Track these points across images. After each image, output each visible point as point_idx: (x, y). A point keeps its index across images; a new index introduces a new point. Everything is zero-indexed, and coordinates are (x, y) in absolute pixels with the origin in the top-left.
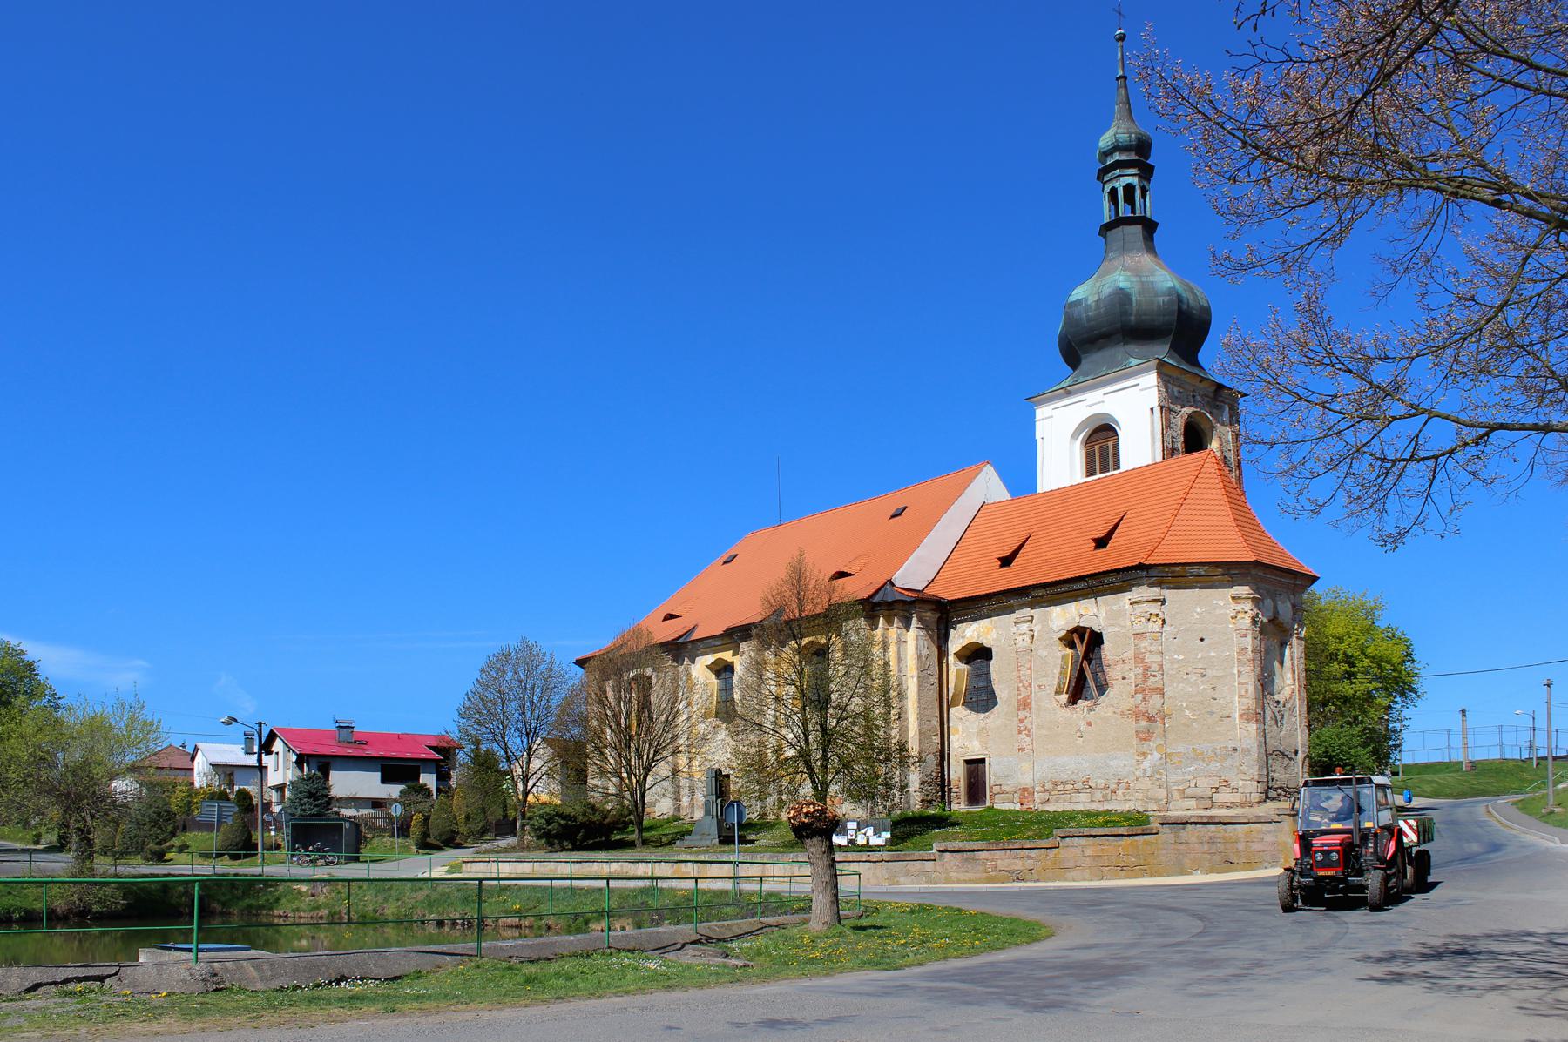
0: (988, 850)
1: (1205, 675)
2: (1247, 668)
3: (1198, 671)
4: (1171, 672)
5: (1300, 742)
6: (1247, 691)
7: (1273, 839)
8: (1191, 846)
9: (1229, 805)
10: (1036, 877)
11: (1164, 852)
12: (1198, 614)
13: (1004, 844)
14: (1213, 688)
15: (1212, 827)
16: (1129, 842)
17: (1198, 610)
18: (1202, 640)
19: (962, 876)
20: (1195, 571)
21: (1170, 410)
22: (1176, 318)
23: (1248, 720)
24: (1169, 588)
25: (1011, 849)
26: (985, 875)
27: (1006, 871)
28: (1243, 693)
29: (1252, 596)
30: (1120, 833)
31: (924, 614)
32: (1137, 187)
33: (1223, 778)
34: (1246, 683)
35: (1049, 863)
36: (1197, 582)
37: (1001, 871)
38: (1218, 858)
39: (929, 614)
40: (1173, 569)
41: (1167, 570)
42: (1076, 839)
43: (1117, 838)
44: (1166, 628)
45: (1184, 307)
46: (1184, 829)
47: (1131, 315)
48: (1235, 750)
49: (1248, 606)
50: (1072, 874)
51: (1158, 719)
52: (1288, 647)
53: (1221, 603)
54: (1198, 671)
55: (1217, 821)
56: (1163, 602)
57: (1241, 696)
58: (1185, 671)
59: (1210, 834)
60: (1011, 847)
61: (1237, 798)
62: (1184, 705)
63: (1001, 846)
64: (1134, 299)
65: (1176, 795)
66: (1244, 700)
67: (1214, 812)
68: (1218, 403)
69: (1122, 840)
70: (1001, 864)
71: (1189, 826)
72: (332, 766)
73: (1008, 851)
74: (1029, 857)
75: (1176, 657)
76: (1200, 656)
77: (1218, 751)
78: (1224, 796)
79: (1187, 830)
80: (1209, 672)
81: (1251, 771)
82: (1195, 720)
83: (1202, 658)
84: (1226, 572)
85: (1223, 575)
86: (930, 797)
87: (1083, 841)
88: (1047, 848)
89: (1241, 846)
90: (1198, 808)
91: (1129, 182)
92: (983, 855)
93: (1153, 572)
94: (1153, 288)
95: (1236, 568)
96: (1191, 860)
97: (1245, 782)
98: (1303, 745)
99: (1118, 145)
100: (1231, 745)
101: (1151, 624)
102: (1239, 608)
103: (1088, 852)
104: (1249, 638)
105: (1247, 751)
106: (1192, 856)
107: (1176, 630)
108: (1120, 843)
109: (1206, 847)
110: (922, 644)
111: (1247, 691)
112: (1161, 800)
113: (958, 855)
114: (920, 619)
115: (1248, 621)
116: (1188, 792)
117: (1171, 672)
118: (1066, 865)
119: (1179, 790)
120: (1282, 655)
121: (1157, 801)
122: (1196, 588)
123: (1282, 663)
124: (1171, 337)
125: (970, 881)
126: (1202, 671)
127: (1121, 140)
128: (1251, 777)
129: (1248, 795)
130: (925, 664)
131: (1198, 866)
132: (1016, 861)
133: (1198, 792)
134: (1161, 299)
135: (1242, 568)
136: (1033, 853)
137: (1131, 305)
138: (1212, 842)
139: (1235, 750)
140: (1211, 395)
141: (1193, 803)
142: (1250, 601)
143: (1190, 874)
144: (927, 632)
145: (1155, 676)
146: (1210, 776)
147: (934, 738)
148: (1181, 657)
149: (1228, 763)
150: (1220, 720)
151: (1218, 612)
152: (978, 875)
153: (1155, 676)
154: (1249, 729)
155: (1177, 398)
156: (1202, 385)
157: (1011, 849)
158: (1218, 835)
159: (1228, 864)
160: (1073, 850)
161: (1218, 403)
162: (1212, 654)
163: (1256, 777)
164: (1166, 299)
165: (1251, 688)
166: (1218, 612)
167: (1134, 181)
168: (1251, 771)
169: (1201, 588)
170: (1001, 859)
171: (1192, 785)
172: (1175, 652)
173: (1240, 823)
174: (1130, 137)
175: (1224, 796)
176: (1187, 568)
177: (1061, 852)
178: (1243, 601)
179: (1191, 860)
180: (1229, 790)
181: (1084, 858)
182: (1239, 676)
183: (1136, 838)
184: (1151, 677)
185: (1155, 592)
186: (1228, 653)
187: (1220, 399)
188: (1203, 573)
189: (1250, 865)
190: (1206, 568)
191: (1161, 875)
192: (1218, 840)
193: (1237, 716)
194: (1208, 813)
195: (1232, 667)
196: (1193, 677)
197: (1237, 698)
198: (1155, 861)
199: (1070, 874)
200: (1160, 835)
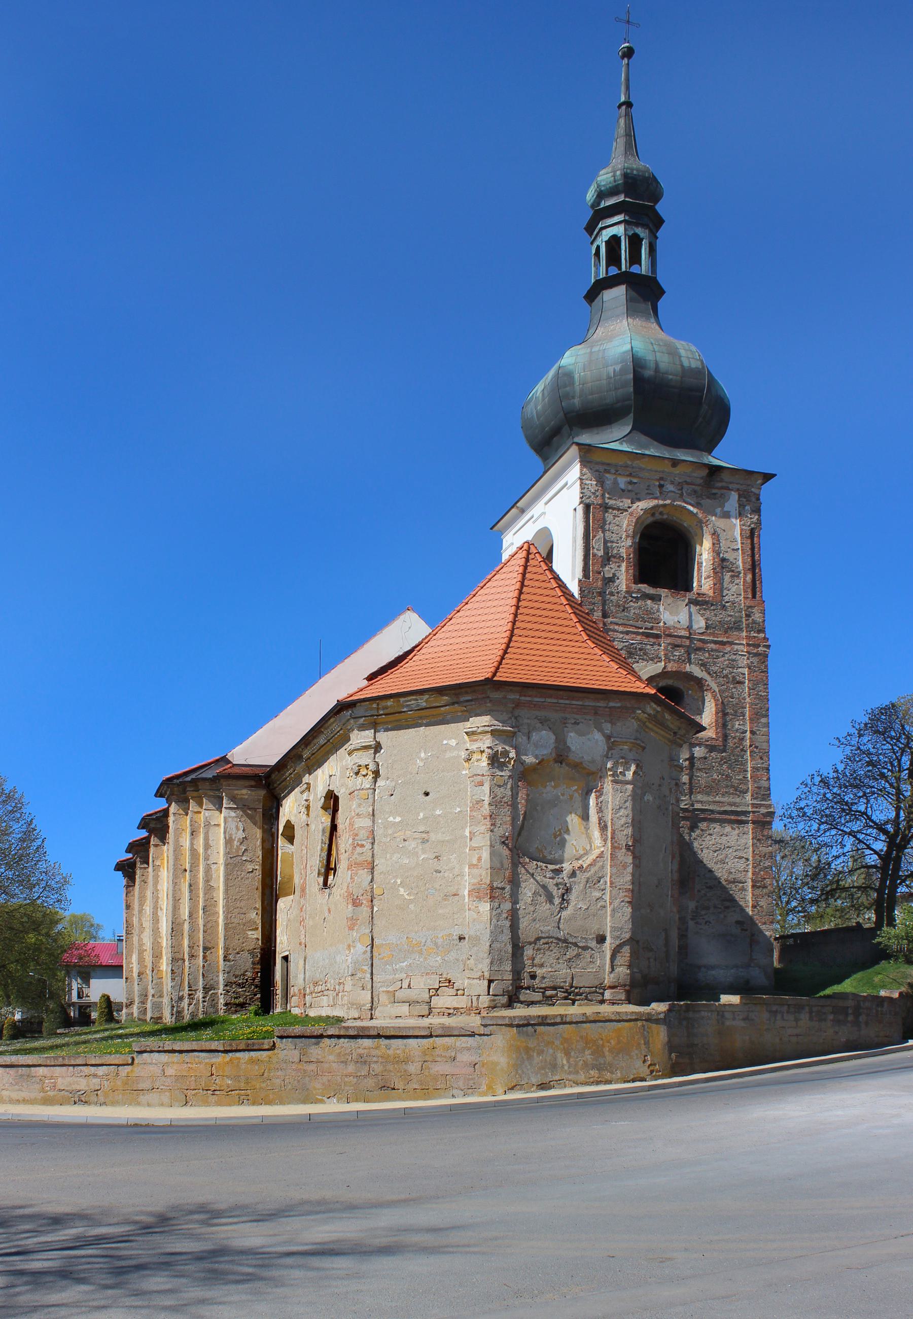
0: (46, 1066)
1: (428, 841)
2: (483, 827)
3: (417, 835)
4: (384, 840)
5: (609, 924)
6: (479, 859)
7: (474, 1058)
8: (326, 1066)
9: (451, 1011)
10: (102, 1099)
11: (280, 1073)
12: (422, 760)
13: (63, 1058)
14: (437, 857)
15: (367, 1042)
16: (228, 1059)
17: (423, 755)
18: (427, 794)
19: (15, 1095)
20: (412, 702)
21: (606, 508)
22: (632, 389)
23: (479, 898)
24: (387, 730)
25: (74, 1066)
26: (42, 1094)
27: (67, 1091)
28: (475, 862)
29: (489, 729)
30: (213, 1048)
31: (236, 792)
32: (623, 238)
33: (444, 976)
34: (480, 848)
35: (119, 1083)
36: (421, 718)
37: (60, 1090)
38: (370, 1082)
39: (244, 791)
40: (383, 703)
41: (375, 706)
42: (156, 1054)
43: (212, 1054)
44: (380, 782)
45: (648, 373)
46: (317, 1044)
47: (573, 397)
48: (461, 938)
49: (487, 742)
50: (147, 1096)
51: (364, 902)
52: (593, 795)
53: (453, 742)
54: (417, 835)
55: (375, 1033)
56: (378, 747)
57: (471, 866)
58: (402, 837)
59: (361, 1051)
60: (73, 1062)
61: (462, 1002)
62: (399, 881)
63: (60, 1061)
64: (576, 376)
65: (384, 998)
66: (475, 871)
67: (435, 1021)
68: (714, 491)
69: (217, 1057)
70: (61, 1083)
71: (326, 1040)
72: (92, 974)
73: (71, 1068)
74: (95, 1076)
75: (391, 819)
76: (421, 815)
77: (440, 941)
78: (444, 1001)
79: (321, 1045)
80: (433, 837)
81: (480, 966)
82: (411, 901)
83: (424, 818)
84: (455, 700)
85: (453, 704)
86: (241, 1000)
87: (164, 1057)
88: (118, 1065)
89: (413, 1068)
90: (411, 1016)
91: (614, 233)
92: (41, 1071)
93: (359, 710)
94: (603, 358)
95: (467, 693)
96: (323, 1084)
97: (471, 981)
98: (613, 929)
99: (601, 191)
100: (457, 932)
101: (360, 778)
102: (474, 747)
103: (170, 1071)
104: (486, 788)
105: (476, 939)
106: (325, 1079)
107: (393, 784)
108: (214, 1060)
109: (351, 1068)
110: (233, 826)
111: (479, 859)
112: (364, 1005)
113: (12, 1071)
114: (233, 799)
115: (484, 763)
116: (400, 995)
117: (384, 840)
118: (141, 1086)
119: (388, 992)
120: (586, 807)
121: (359, 1007)
122: (420, 725)
123: (585, 817)
124: (632, 415)
125: (25, 1101)
126: (424, 835)
127: (603, 183)
128: (480, 974)
129: (474, 999)
130: (238, 848)
131: (334, 1091)
132: (81, 1079)
133: (412, 994)
134: (611, 369)
135: (474, 691)
136: (101, 1071)
137: (573, 384)
138: (362, 1061)
139: (461, 938)
140: (700, 481)
141: (404, 1009)
142: (489, 735)
143: (321, 1101)
144: (244, 812)
145: (362, 846)
146: (427, 974)
147: (250, 933)
148: (398, 819)
149: (452, 955)
150: (445, 900)
151: (448, 755)
152: (33, 1095)
153: (362, 846)
154: (481, 910)
155: (623, 491)
156: (677, 470)
157: (74, 1066)
158: (374, 1052)
159: (386, 1089)
160: (151, 1068)
161: (714, 491)
162: (438, 812)
163: (487, 975)
164: (618, 368)
165: (486, 855)
166: (448, 755)
167: (619, 230)
168: (480, 966)
169: (427, 725)
170: (63, 1077)
171: (405, 985)
172: (391, 813)
173: (416, 1037)
174: (614, 176)
175: (444, 1001)
176: (402, 700)
177: (137, 1070)
178: (481, 737)
179: (323, 1084)
180: (453, 992)
181: (163, 1079)
182: (471, 839)
183: (238, 1055)
184: (358, 848)
185: (367, 737)
186: (458, 809)
187: (719, 485)
188: (424, 704)
189: (425, 1092)
190: (426, 697)
191: (269, 1102)
192: (375, 1059)
193: (466, 893)
194: (426, 1022)
195: (463, 828)
196: (411, 845)
197: (467, 870)
198: (264, 1085)
199: (143, 1098)
200: (276, 1051)
